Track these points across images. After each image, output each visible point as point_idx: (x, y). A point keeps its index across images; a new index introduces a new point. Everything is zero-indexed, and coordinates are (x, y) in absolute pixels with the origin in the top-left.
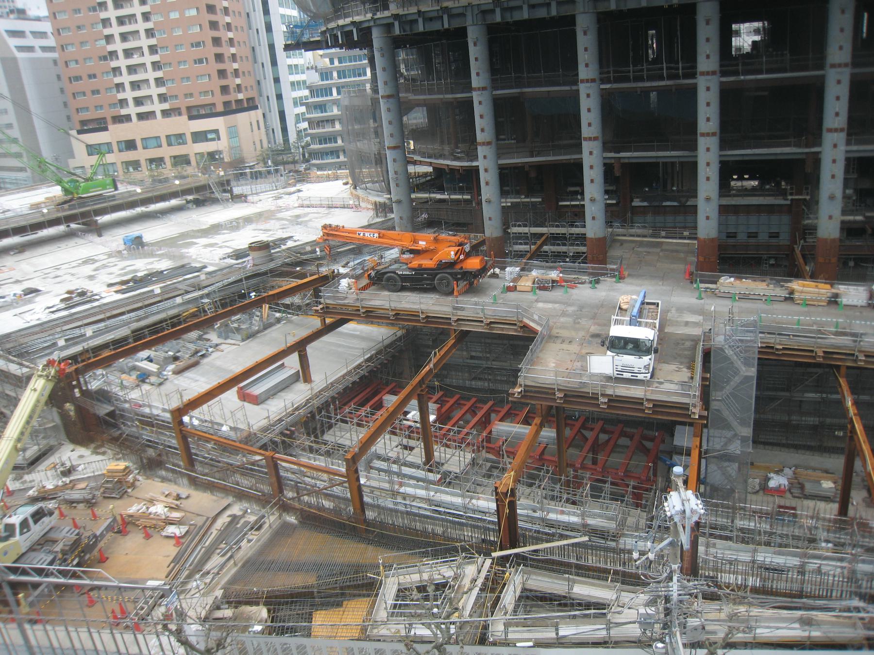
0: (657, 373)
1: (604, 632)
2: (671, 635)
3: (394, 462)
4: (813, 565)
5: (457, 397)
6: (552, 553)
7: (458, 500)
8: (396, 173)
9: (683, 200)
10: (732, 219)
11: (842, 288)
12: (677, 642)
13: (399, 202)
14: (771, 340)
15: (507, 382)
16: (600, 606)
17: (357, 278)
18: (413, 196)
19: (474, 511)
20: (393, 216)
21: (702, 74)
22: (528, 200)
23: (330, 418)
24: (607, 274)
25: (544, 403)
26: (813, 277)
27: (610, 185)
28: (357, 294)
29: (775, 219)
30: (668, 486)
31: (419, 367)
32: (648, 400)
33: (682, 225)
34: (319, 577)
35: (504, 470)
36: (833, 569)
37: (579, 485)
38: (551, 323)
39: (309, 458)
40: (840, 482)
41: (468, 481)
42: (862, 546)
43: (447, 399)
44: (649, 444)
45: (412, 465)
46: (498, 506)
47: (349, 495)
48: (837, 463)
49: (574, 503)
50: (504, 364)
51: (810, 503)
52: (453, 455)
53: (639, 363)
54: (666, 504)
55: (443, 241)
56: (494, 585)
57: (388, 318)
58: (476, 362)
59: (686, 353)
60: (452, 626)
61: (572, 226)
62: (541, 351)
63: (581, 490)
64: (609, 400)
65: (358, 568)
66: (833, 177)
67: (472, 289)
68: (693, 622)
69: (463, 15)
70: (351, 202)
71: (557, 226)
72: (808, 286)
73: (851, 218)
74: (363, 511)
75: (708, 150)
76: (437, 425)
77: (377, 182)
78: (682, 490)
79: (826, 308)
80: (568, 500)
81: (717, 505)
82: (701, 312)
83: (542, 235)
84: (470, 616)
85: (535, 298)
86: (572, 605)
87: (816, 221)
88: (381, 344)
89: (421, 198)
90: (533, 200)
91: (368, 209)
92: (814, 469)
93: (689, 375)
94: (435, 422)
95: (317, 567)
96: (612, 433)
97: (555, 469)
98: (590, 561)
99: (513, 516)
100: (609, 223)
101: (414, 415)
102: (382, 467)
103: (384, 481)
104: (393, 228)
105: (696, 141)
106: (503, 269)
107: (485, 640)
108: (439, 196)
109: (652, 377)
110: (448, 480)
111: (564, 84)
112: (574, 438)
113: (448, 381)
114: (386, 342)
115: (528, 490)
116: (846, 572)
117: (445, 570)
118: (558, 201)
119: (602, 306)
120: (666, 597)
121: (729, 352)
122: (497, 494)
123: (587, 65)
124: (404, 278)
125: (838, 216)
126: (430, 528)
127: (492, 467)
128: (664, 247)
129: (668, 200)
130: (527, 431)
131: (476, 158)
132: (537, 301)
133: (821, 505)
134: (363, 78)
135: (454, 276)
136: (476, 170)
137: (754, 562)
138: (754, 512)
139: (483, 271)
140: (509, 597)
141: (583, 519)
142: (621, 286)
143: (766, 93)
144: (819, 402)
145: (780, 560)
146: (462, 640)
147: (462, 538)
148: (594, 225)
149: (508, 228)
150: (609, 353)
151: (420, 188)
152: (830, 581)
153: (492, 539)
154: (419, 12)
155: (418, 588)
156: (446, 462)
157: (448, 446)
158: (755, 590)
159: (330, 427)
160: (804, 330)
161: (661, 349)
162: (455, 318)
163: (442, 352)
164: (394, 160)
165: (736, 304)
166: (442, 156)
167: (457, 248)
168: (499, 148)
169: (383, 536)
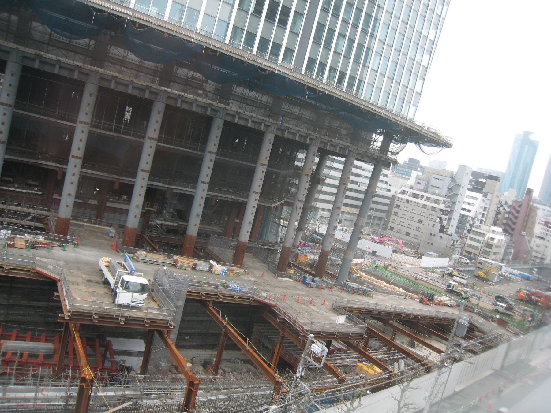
21: (81, 122)
32: (147, 319)
105: (68, 160)
123: (213, 144)
142: (78, 250)
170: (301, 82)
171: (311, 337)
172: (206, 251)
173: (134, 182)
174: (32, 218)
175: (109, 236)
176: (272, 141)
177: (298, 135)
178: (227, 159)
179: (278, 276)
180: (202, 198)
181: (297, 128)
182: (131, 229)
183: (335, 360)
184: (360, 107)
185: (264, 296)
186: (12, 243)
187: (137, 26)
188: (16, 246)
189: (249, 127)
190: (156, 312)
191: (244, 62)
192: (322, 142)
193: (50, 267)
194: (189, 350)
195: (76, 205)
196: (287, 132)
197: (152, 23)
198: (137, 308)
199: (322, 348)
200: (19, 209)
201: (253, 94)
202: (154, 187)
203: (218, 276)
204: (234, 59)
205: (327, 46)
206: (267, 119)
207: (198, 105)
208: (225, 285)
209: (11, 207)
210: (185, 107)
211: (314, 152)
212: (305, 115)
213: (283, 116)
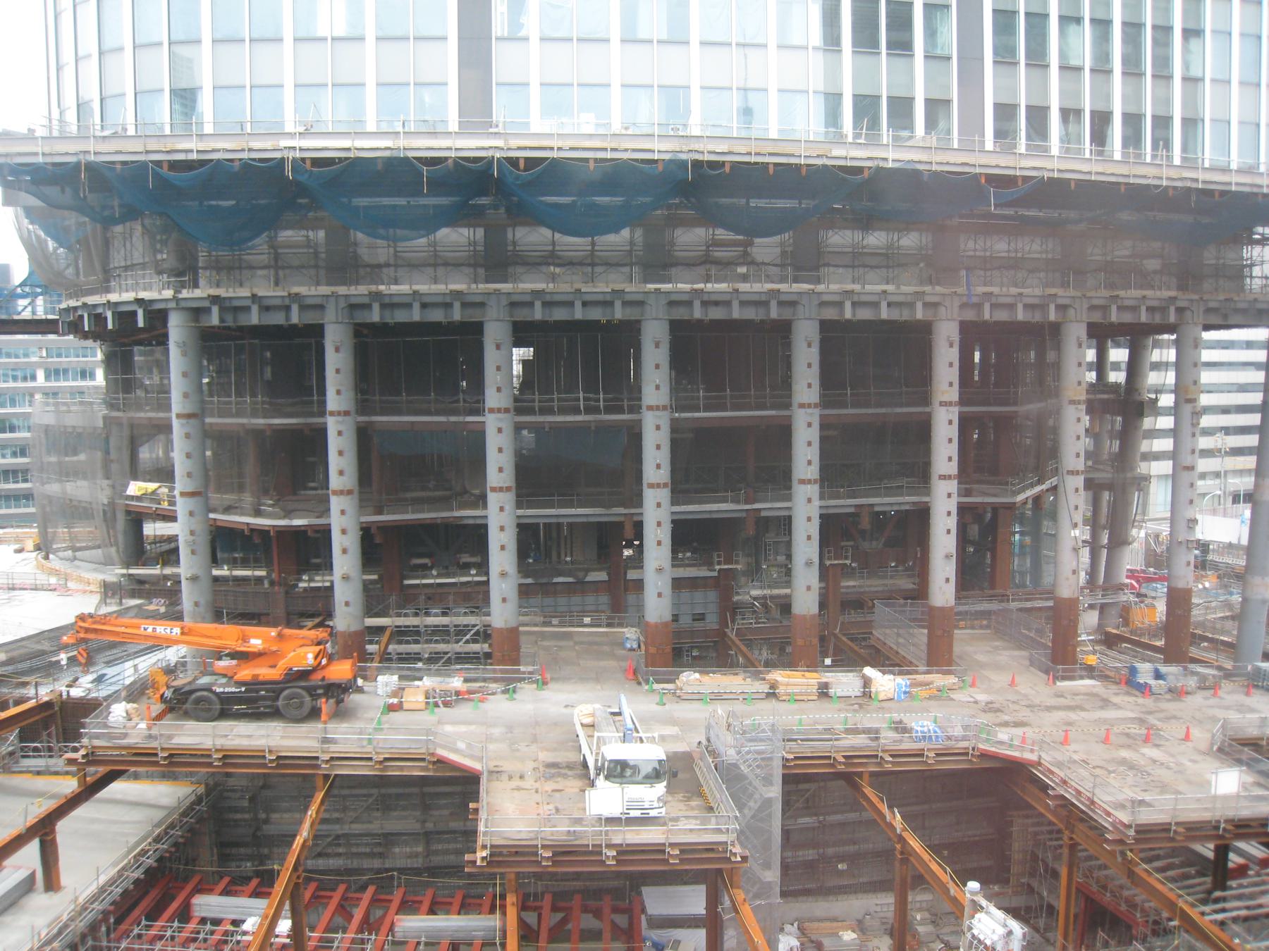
9: (581, 574)
10: (685, 595)
21: (492, 411)
24: (524, 679)
29: (699, 596)
33: (580, 608)
61: (427, 614)
67: (341, 713)
69: (321, 307)
79: (818, 703)
111: (438, 413)
118: (404, 577)
123: (338, 392)
124: (226, 699)
128: (577, 639)
129: (560, 575)
134: (30, 384)
142: (545, 693)
144: (814, 829)
148: (502, 608)
154: (254, 296)
162: (326, 757)
167: (318, 648)
170: (967, 169)
171: (972, 893)
172: (872, 642)
174: (475, 634)
175: (624, 648)
176: (956, 338)
177: (1143, 309)
178: (870, 411)
179: (1056, 678)
180: (809, 519)
181: (1014, 291)
182: (656, 625)
184: (1157, 187)
185: (1006, 741)
186: (395, 701)
187: (522, 165)
188: (406, 706)
189: (919, 321)
190: (693, 824)
191: (798, 166)
192: (1093, 308)
193: (461, 745)
194: (852, 897)
195: (524, 591)
196: (1114, 308)
197: (552, 149)
198: (645, 821)
199: (1005, 926)
200: (444, 620)
201: (876, 239)
202: (715, 516)
204: (771, 168)
205: (1163, 76)
206: (928, 289)
207: (743, 304)
208: (901, 728)
209: (431, 620)
210: (716, 314)
211: (1078, 338)
212: (1029, 252)
213: (968, 269)
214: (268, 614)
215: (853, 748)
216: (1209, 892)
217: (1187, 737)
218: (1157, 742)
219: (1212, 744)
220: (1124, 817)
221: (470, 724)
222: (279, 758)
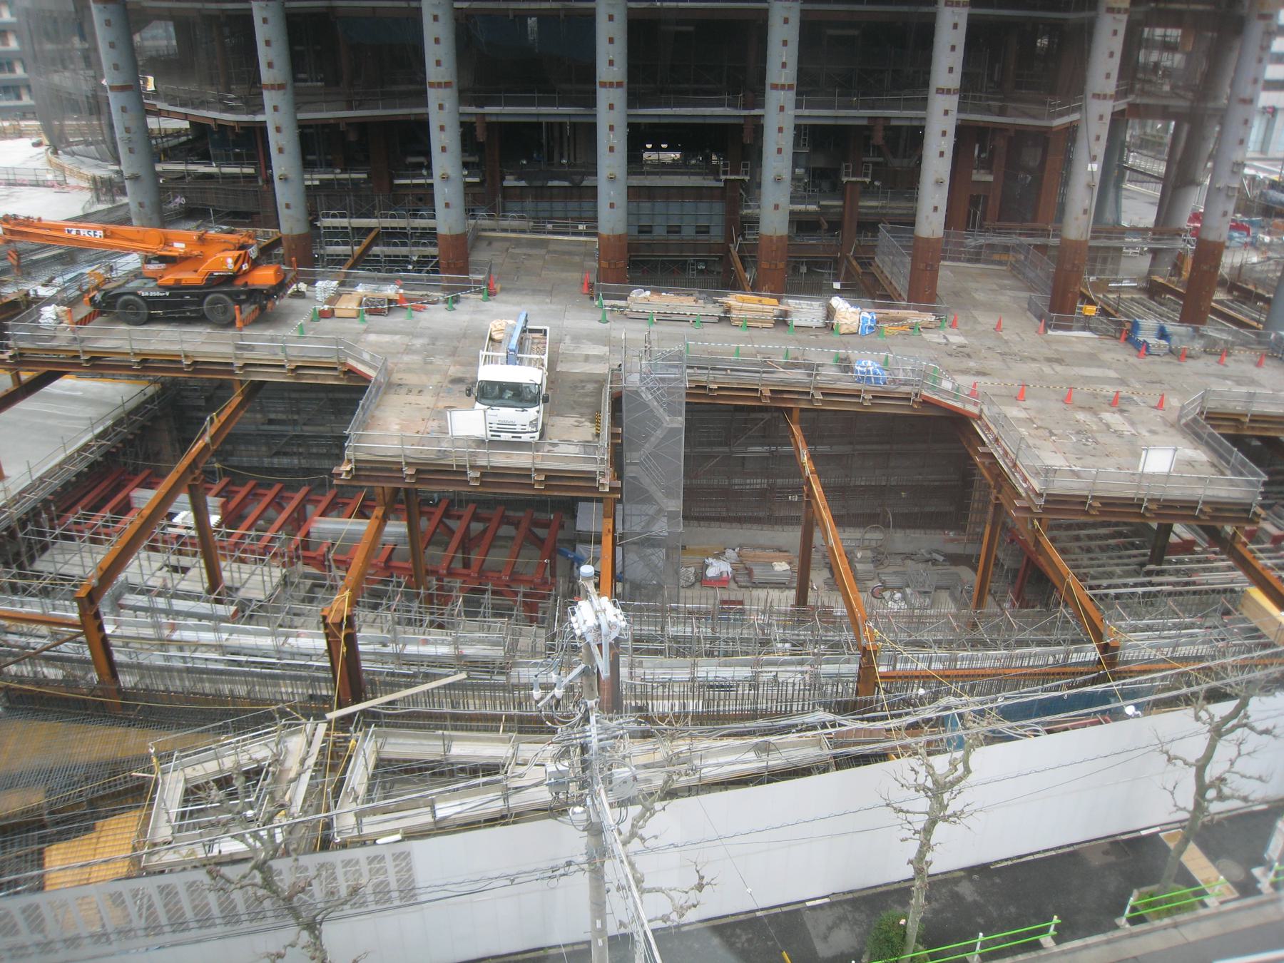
0: (549, 430)
1: (500, 803)
2: (594, 795)
3: (159, 594)
4: (767, 674)
5: (252, 483)
6: (416, 703)
7: (267, 642)
8: (127, 130)
9: (577, 178)
10: (646, 206)
11: (792, 304)
12: (601, 803)
13: (135, 178)
14: (703, 377)
15: (327, 456)
16: (491, 769)
17: (71, 303)
18: (159, 168)
19: (293, 655)
20: (125, 200)
22: (346, 176)
23: (42, 534)
24: (469, 288)
25: (386, 485)
26: (755, 288)
27: (470, 155)
28: (73, 331)
29: (704, 206)
30: (574, 593)
31: (186, 443)
34: (50, 792)
35: (333, 588)
36: (792, 675)
37: (446, 600)
38: (390, 365)
39: (12, 603)
40: (797, 562)
41: (278, 610)
42: (825, 642)
43: (235, 488)
44: (541, 532)
45: (187, 596)
46: (329, 643)
47: (88, 654)
48: (791, 536)
49: (441, 626)
50: (321, 428)
51: (761, 593)
52: (253, 573)
53: (522, 418)
54: (573, 619)
55: (213, 241)
56: (334, 760)
57: (129, 368)
58: (278, 428)
59: (588, 399)
60: (278, 830)
61: (415, 216)
62: (378, 406)
63: (449, 607)
64: (482, 474)
65: (116, 767)
66: (779, 151)
67: (264, 317)
68: (621, 773)
70: (50, 177)
71: (393, 217)
72: (750, 302)
73: (802, 207)
74: (114, 676)
75: (611, 107)
76: (224, 530)
77: (91, 144)
78: (594, 597)
80: (431, 624)
81: (640, 609)
82: (605, 340)
83: (370, 229)
84: (304, 812)
85: (363, 326)
86: (452, 773)
87: (757, 211)
88: (120, 410)
89: (173, 172)
90: (354, 176)
91: (82, 189)
92: (764, 548)
93: (594, 431)
94: (219, 525)
95: (43, 776)
96: (489, 520)
97: (416, 582)
98: (472, 708)
99: (353, 656)
100: (470, 212)
101: (184, 517)
102: (140, 604)
103: (145, 625)
104: (127, 221)
105: (595, 92)
106: (311, 283)
107: (329, 842)
108: (202, 169)
109: (541, 437)
110: (248, 613)
112: (434, 532)
113: (234, 460)
114: (131, 405)
115: (371, 615)
116: (807, 677)
117: (258, 748)
118: (392, 178)
119: (465, 336)
120: (582, 745)
121: (647, 397)
122: (326, 626)
124: (151, 303)
125: (786, 206)
126: (226, 689)
127: (314, 585)
128: (551, 247)
130: (364, 528)
131: (260, 108)
132: (366, 331)
133: (775, 594)
135: (235, 296)
136: (262, 128)
137: (693, 680)
138: (690, 613)
139: (281, 287)
140: (358, 776)
141: (457, 648)
142: (492, 305)
143: (691, 28)
145: (726, 673)
146: (295, 850)
147: (278, 697)
148: (447, 216)
149: (317, 219)
150: (478, 405)
151: (170, 154)
152: (790, 692)
153: (324, 692)
155: (217, 781)
156: (243, 586)
157: (242, 561)
158: (700, 719)
159: (44, 548)
160: (744, 363)
161: (554, 396)
162: (240, 363)
163: (223, 417)
164: (124, 110)
165: (654, 328)
166: (203, 104)
167: (237, 253)
168: (297, 93)
169: (151, 711)
173: (924, 119)
179: (1048, 327)
183: (1188, 573)
185: (952, 389)
188: (337, 313)
203: (840, 342)
214: (258, 213)
215: (782, 382)
216: (1142, 565)
217: (1160, 406)
218: (1124, 408)
219: (1180, 418)
220: (1037, 485)
221: (396, 333)
222: (195, 363)
